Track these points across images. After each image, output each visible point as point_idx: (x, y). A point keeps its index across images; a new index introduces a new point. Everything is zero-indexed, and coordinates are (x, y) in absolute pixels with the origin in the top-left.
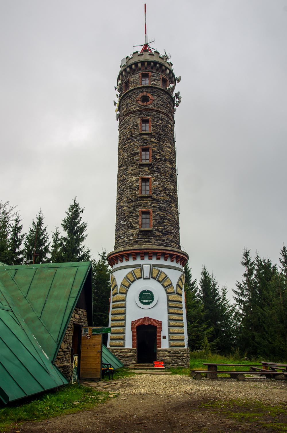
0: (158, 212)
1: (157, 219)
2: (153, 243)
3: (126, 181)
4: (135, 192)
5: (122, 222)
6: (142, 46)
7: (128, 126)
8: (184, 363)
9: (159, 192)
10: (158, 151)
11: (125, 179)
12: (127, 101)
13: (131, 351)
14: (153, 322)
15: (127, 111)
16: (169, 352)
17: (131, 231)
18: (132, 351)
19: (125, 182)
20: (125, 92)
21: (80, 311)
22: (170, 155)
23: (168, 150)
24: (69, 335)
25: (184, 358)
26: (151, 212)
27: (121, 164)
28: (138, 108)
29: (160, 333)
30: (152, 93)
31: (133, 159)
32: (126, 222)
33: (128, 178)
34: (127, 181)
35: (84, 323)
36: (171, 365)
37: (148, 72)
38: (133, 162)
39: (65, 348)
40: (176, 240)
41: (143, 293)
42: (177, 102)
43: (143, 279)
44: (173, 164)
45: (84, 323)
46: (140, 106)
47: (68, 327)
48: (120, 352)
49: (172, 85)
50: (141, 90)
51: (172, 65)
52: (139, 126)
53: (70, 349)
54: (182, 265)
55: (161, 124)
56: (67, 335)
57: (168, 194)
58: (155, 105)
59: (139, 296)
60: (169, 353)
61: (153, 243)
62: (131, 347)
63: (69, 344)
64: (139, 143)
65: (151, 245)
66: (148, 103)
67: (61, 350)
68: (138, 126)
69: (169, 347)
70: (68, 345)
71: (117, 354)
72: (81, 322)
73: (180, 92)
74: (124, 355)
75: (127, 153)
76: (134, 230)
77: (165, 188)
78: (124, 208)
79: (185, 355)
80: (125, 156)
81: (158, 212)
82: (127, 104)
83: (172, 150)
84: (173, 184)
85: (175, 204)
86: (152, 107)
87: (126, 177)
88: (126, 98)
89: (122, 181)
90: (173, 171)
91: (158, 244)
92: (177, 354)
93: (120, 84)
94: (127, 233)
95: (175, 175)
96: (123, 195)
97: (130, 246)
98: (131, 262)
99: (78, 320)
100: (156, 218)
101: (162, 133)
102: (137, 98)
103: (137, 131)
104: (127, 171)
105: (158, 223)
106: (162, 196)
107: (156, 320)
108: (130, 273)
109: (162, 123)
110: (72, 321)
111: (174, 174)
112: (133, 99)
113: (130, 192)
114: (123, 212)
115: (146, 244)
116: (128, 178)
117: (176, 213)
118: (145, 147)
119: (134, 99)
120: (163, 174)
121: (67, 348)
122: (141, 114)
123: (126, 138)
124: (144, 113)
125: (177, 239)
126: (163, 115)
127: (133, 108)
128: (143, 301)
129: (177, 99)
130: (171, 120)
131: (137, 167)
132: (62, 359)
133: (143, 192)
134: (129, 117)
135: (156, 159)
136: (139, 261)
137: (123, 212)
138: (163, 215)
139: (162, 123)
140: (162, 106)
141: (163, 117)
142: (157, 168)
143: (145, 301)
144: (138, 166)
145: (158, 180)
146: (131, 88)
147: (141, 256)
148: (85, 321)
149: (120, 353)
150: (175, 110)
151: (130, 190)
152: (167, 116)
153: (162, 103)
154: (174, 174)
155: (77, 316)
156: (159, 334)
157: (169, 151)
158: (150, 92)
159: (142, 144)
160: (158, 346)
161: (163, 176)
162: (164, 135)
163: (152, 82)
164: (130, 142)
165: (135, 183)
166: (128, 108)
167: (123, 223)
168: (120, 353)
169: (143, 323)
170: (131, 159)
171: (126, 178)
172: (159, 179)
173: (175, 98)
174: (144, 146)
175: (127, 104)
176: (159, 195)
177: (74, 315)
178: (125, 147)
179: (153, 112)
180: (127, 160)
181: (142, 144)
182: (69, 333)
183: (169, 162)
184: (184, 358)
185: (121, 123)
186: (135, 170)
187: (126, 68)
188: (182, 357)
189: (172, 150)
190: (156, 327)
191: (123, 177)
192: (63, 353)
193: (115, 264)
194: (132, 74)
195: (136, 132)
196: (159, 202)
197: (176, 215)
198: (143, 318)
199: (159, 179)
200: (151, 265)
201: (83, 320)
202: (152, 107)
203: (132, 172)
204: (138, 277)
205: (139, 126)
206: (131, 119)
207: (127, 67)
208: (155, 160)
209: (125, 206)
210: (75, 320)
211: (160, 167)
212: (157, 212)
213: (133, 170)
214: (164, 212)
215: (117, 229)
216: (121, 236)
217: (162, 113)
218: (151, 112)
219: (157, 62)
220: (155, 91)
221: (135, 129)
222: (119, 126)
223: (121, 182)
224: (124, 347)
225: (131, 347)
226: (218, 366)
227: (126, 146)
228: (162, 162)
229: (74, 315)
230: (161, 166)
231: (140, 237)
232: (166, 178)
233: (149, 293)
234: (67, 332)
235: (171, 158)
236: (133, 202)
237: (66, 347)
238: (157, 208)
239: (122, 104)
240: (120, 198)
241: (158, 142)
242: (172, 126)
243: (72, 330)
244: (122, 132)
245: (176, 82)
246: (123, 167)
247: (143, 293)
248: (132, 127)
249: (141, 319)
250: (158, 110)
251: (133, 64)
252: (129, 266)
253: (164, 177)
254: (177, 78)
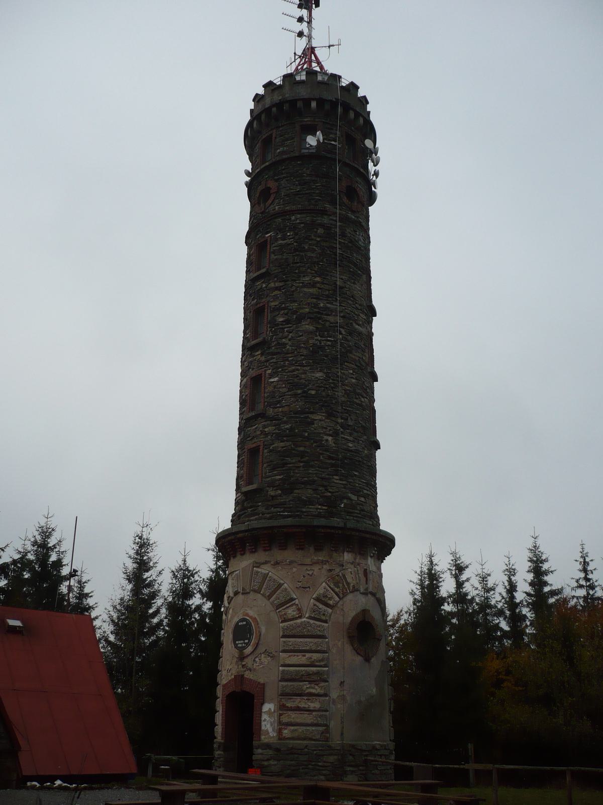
0: (275, 445)
16: (278, 750)
81: (275, 445)
91: (268, 516)
92: (296, 756)
105: (274, 469)
109: (296, 234)
135: (278, 325)
138: (284, 447)
147: (365, 103)
176: (278, 405)
199: (280, 370)
211: (284, 340)
212: (274, 444)
214: (287, 441)
217: (292, 212)
228: (291, 327)
230: (286, 338)
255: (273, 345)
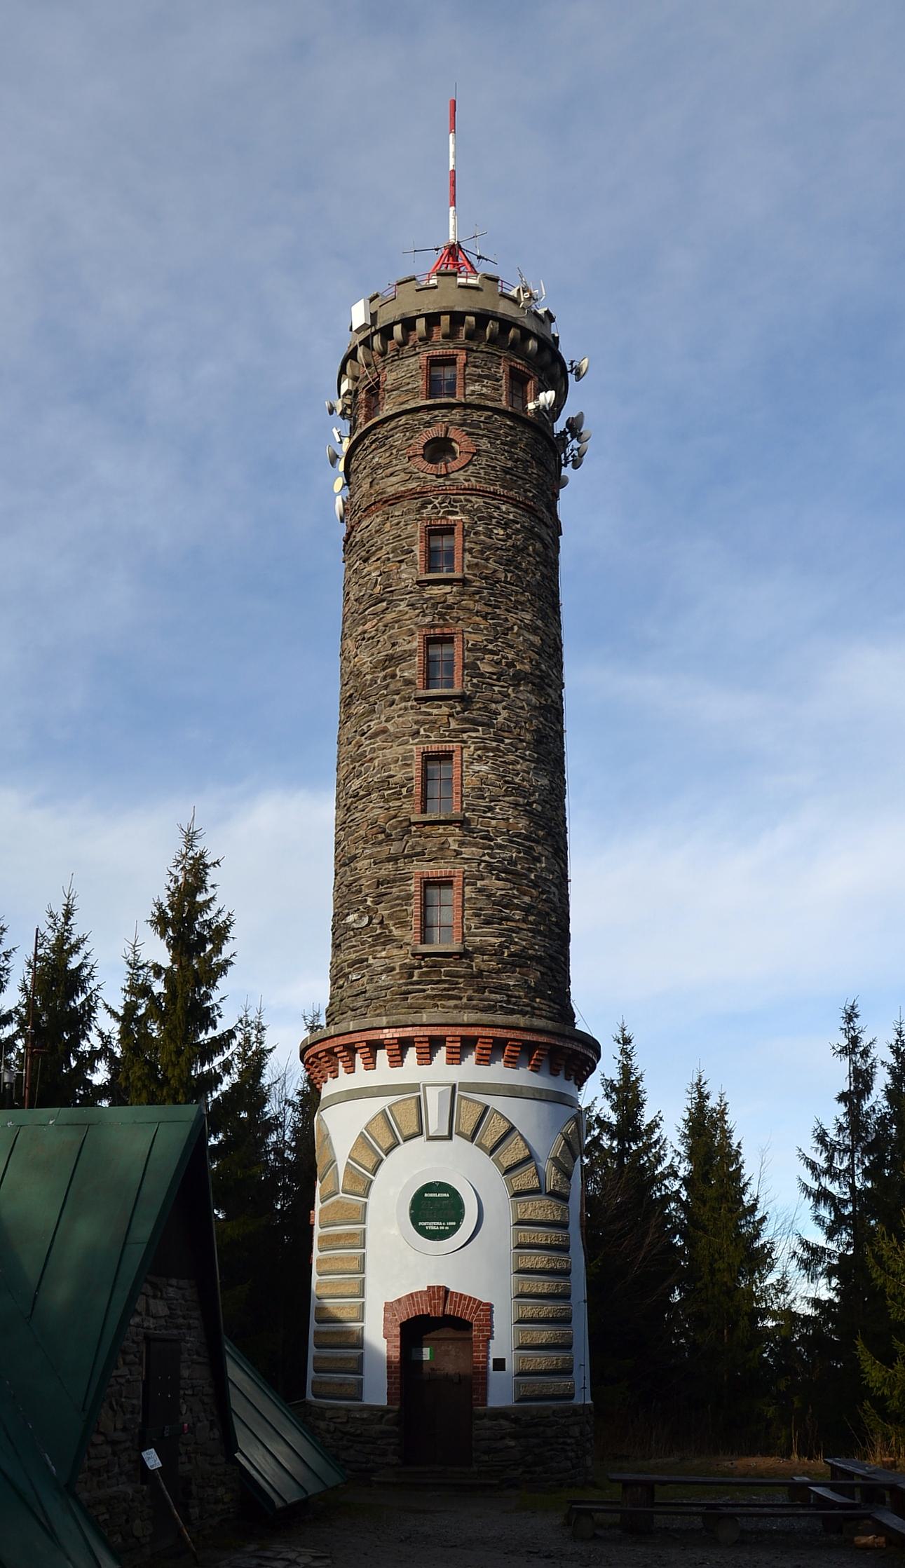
1: (480, 909)
2: (465, 1000)
3: (366, 762)
4: (398, 803)
5: (351, 918)
6: (437, 250)
7: (376, 551)
8: (569, 1464)
9: (492, 804)
10: (490, 647)
11: (363, 755)
12: (373, 458)
13: (382, 1416)
14: (459, 1307)
15: (372, 495)
16: (516, 1421)
17: (384, 954)
18: (387, 1417)
19: (362, 765)
20: (366, 422)
21: (172, 1286)
22: (537, 657)
23: (529, 639)
24: (128, 1381)
25: (569, 1441)
26: (457, 881)
27: (351, 696)
28: (414, 485)
29: (487, 1347)
30: (470, 425)
31: (393, 676)
32: (366, 920)
33: (373, 750)
34: (372, 760)
35: (189, 1327)
36: (520, 1470)
37: (455, 351)
38: (392, 687)
39: (115, 1429)
40: (555, 984)
41: (426, 1195)
42: (572, 450)
43: (423, 1139)
44: (550, 691)
45: (189, 1327)
46: (422, 475)
47: (125, 1352)
48: (345, 1420)
49: (548, 397)
50: (427, 418)
51: (552, 320)
52: (417, 552)
53: (137, 1430)
54: (572, 1081)
55: (504, 541)
56: (122, 1381)
57: (526, 811)
58: (482, 471)
59: (411, 1208)
60: (514, 1425)
61: (465, 1000)
62: (383, 1401)
63: (132, 1413)
64: (418, 616)
65: (456, 1007)
66: (454, 465)
67: (98, 1439)
68: (412, 551)
69: (516, 1402)
70: (129, 1416)
71: (336, 1428)
72: (178, 1327)
73: (585, 415)
74: (359, 1432)
75: (373, 655)
76: (395, 952)
77: (513, 788)
78: (359, 865)
79: (575, 1431)
80: (364, 663)
82: (374, 469)
83: (544, 637)
84: (548, 767)
85: (552, 846)
86: (469, 480)
87: (367, 745)
88: (372, 443)
89: (353, 762)
90: (546, 720)
93: (348, 392)
94: (371, 961)
95: (557, 732)
96: (357, 815)
97: (378, 1012)
98: (383, 1072)
99: (163, 1322)
100: (479, 906)
101: (506, 577)
102: (410, 446)
103: (409, 570)
104: (371, 721)
105: (488, 923)
106: (500, 817)
107: (470, 1298)
108: (380, 1116)
110: (138, 1326)
111: (552, 729)
112: (394, 451)
113: (381, 804)
114: (355, 881)
115: (439, 1003)
116: (373, 750)
117: (556, 882)
118: (438, 631)
119: (398, 451)
120: (506, 734)
121: (124, 1429)
122: (423, 506)
123: (366, 597)
124: (436, 502)
125: (557, 981)
126: (512, 509)
127: (392, 485)
128: (425, 1224)
129: (575, 440)
130: (545, 524)
131: (406, 709)
132: (108, 1472)
133: (428, 800)
134: (379, 520)
135: (482, 675)
136: (411, 1069)
137: (355, 881)
139: (509, 537)
140: (507, 473)
141: (511, 517)
142: (486, 708)
143: (432, 1226)
144: (410, 704)
145: (487, 757)
146: (387, 409)
148: (191, 1322)
149: (347, 1422)
150: (562, 482)
151: (383, 796)
152: (527, 511)
153: (510, 464)
154: (552, 729)
155: (160, 1308)
156: (481, 1351)
157: (532, 644)
158: (461, 425)
159: (428, 619)
160: (477, 1399)
161: (507, 741)
162: (512, 584)
163: (472, 388)
164: (383, 612)
165: (401, 769)
166: (376, 482)
167: (355, 921)
168: (347, 1422)
169: (425, 1309)
170: (385, 678)
171: (368, 749)
172: (492, 754)
173: (569, 436)
174: (433, 627)
175: (374, 469)
176: (489, 815)
177: (147, 1304)
178: (365, 632)
179: (473, 499)
180: (371, 680)
181: (428, 619)
182: (128, 1372)
183: (533, 684)
184: (569, 1441)
185: (351, 539)
186: (401, 719)
187: (368, 336)
188: (561, 1440)
189: (544, 637)
190: (471, 1325)
191: (357, 742)
192: (109, 1449)
193: (330, 1079)
194: (393, 356)
195: (404, 576)
196: (491, 840)
197: (553, 889)
198: (426, 1289)
200: (454, 1086)
201: (184, 1317)
202: (469, 480)
203: (389, 725)
204: (406, 1133)
205: (417, 552)
206: (388, 524)
207: (373, 334)
208: (475, 681)
209: (365, 858)
210: (150, 1323)
213: (393, 718)
215: (338, 942)
216: (350, 973)
218: (462, 497)
219: (490, 313)
220: (482, 419)
221: (401, 561)
222: (344, 546)
223: (348, 764)
224: (361, 1400)
225: (383, 1401)
226: (656, 1486)
227: (366, 627)
229: (147, 1304)
231: (415, 978)
232: (517, 749)
233: (445, 1195)
234: (123, 1370)
235: (541, 671)
236: (393, 840)
237: (119, 1426)
238: (483, 864)
239: (354, 465)
240: (345, 823)
241: (489, 610)
242: (546, 546)
243: (141, 1359)
244: (355, 571)
245: (571, 377)
246: (358, 708)
247: (426, 1195)
248: (391, 556)
249: (416, 1293)
250: (490, 492)
251: (395, 323)
252: (375, 1090)
253: (511, 744)
254: (574, 365)
255: (475, 708)
